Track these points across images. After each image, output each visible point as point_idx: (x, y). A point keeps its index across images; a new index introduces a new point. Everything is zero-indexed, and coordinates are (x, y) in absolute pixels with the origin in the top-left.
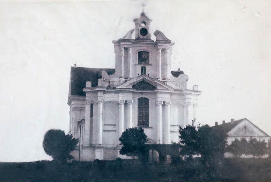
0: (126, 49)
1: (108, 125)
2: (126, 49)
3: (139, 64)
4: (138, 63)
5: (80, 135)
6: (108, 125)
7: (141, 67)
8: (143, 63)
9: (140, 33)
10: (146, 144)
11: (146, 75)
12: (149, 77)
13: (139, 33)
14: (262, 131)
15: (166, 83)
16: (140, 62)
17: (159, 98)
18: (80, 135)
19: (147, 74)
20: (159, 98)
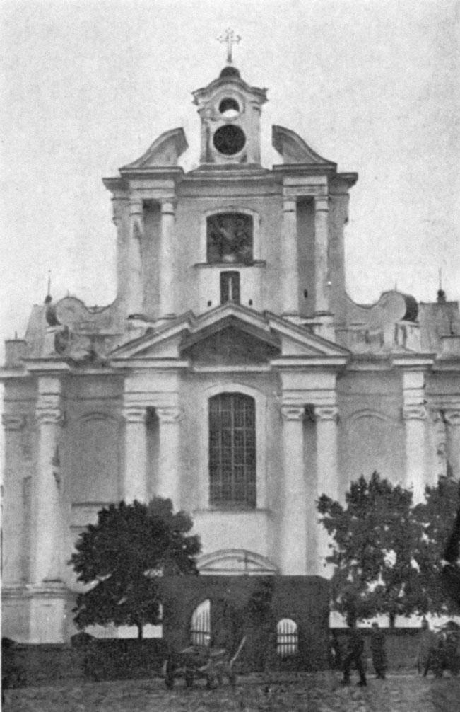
0: (151, 208)
1: (415, 389)
2: (151, 208)
3: (211, 262)
4: (204, 260)
5: (316, 390)
6: (415, 389)
7: (219, 275)
8: (229, 258)
9: (215, 144)
10: (204, 576)
11: (243, 306)
12: (249, 312)
13: (211, 142)
14: (326, 340)
15: (316, 330)
16: (217, 256)
17: (418, 389)
18: (316, 390)
19: (244, 301)
20: (418, 389)
